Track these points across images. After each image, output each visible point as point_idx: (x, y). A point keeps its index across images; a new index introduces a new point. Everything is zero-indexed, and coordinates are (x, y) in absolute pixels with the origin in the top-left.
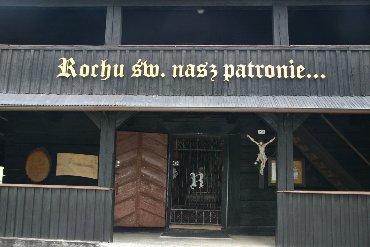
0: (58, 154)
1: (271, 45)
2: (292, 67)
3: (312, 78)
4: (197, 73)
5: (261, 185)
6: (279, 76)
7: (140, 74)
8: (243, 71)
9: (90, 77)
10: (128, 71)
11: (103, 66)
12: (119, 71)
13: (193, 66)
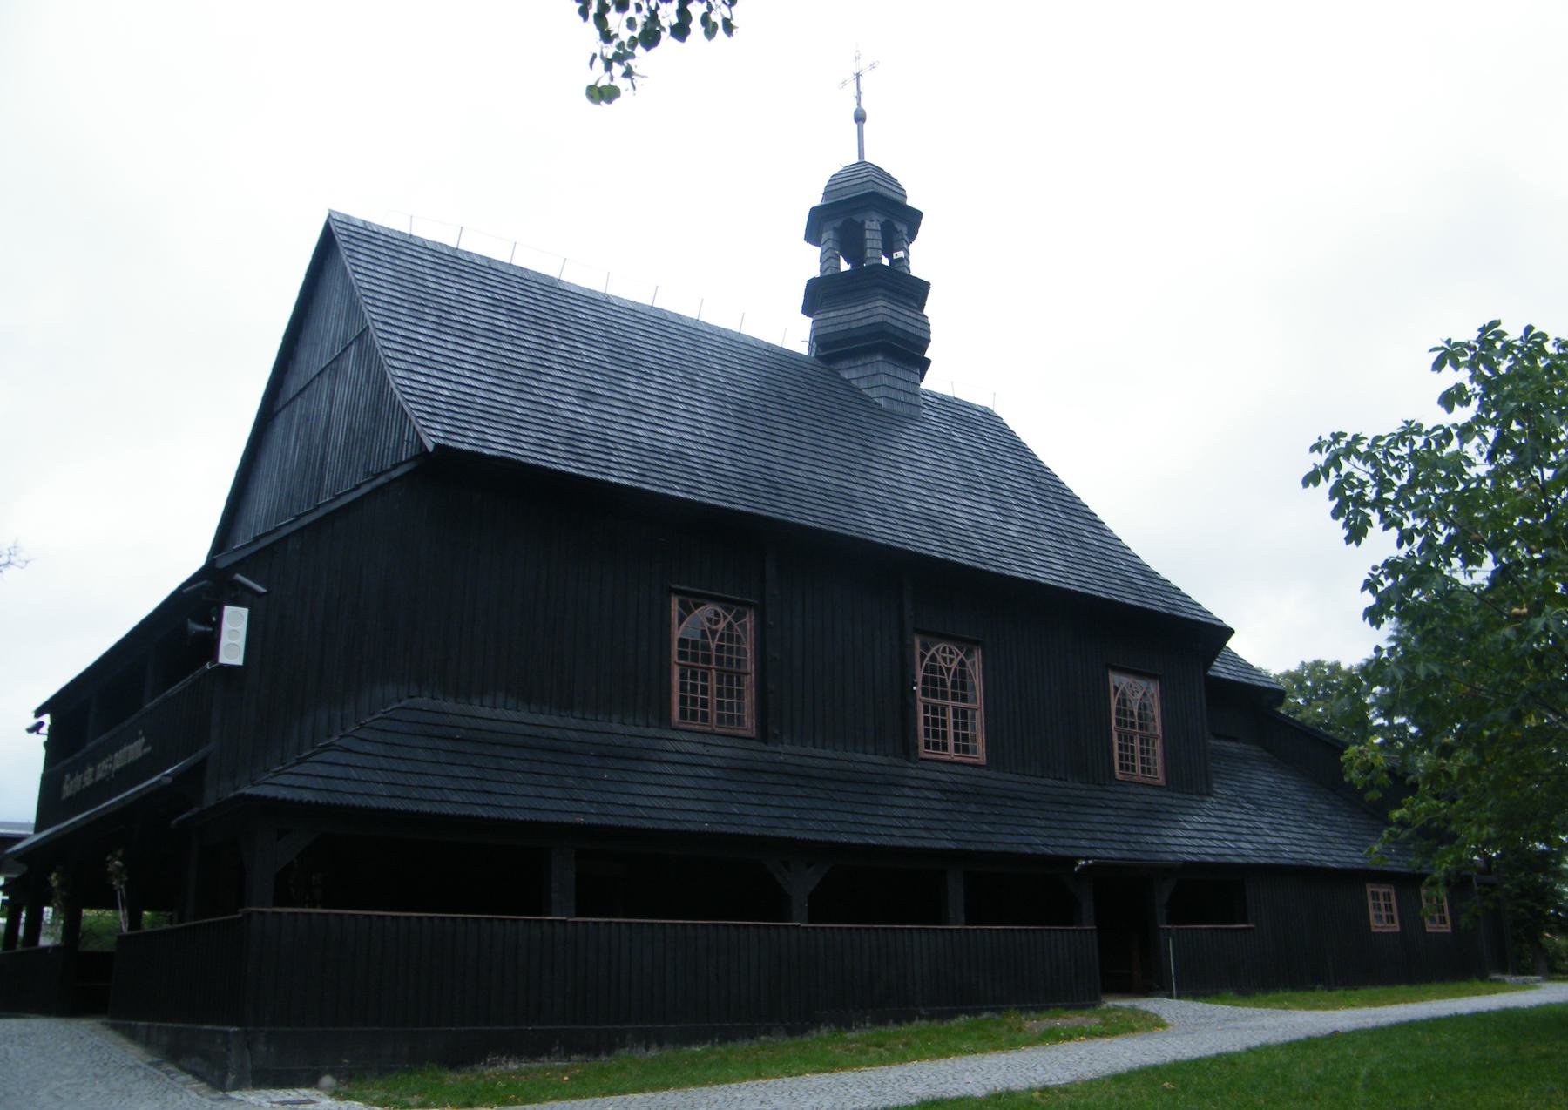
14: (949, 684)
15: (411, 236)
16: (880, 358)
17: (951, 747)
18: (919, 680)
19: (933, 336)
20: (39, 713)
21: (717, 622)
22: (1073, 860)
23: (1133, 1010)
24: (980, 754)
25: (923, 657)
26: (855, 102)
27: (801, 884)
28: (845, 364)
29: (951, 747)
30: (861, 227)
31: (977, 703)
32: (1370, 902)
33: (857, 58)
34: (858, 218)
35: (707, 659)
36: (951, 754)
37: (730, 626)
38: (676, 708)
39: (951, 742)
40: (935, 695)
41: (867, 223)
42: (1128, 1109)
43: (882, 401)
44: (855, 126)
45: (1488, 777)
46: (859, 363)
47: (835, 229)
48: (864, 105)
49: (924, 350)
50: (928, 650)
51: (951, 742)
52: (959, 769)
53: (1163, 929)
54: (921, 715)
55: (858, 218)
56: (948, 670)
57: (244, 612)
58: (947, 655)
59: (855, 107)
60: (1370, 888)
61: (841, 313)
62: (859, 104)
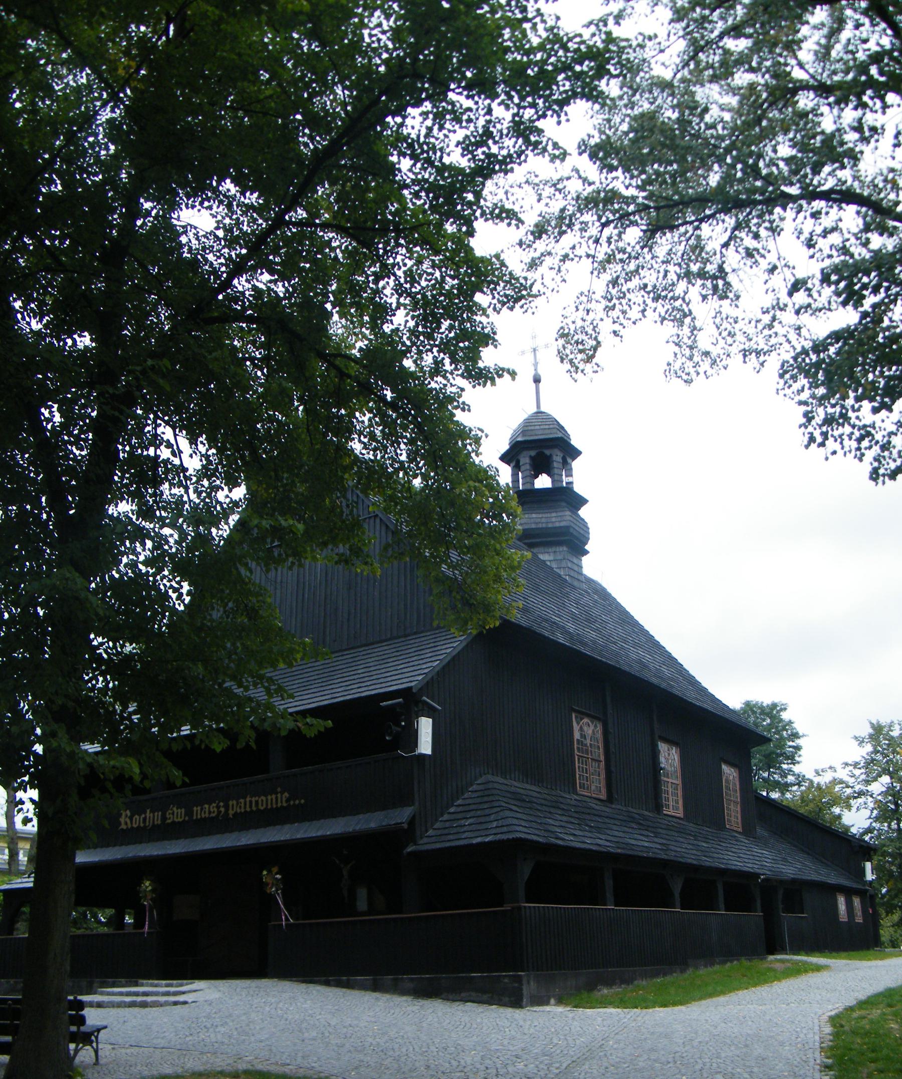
0: (430, 720)
1: (433, 850)
2: (279, 795)
3: (300, 804)
4: (210, 812)
5: (393, 199)
6: (269, 807)
7: (129, 826)
8: (243, 805)
9: (139, 827)
10: (164, 818)
11: (148, 815)
12: (157, 817)
13: (207, 806)
16: (565, 549)
19: (591, 536)
22: (757, 875)
23: (806, 963)
26: (533, 368)
27: (677, 887)
28: (541, 549)
33: (534, 337)
34: (547, 452)
43: (567, 578)
44: (534, 385)
46: (550, 550)
47: (531, 457)
48: (540, 372)
49: (586, 544)
52: (674, 820)
53: (525, 907)
57: (430, 720)
59: (533, 373)
61: (540, 516)
62: (536, 365)
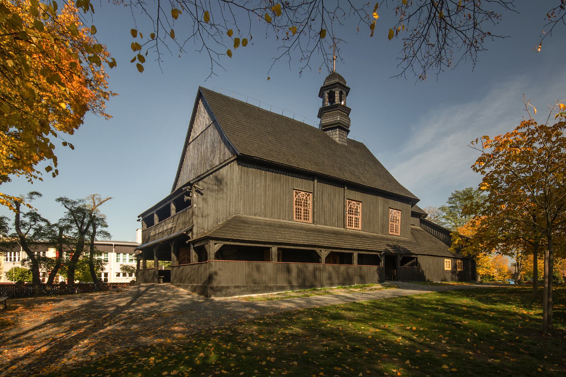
14: (354, 211)
15: (221, 94)
17: (354, 226)
18: (347, 210)
20: (139, 217)
21: (304, 197)
24: (360, 228)
25: (348, 205)
29: (354, 226)
30: (334, 93)
31: (360, 217)
32: (445, 263)
34: (333, 90)
35: (301, 205)
36: (353, 228)
37: (306, 197)
38: (295, 216)
39: (354, 225)
40: (351, 214)
41: (336, 91)
42: (406, 3)
45: (51, 118)
50: (350, 204)
51: (354, 225)
54: (348, 219)
55: (333, 90)
56: (354, 208)
58: (354, 205)
60: (446, 260)
